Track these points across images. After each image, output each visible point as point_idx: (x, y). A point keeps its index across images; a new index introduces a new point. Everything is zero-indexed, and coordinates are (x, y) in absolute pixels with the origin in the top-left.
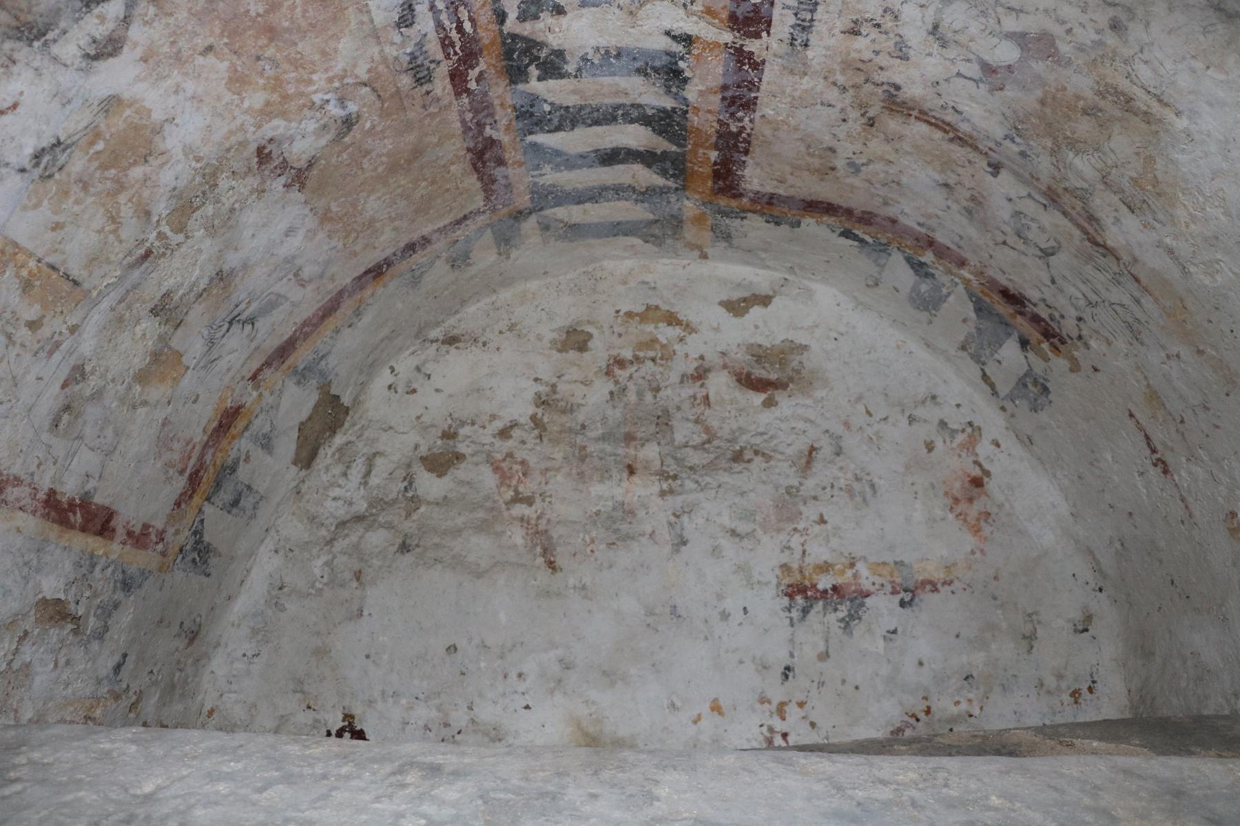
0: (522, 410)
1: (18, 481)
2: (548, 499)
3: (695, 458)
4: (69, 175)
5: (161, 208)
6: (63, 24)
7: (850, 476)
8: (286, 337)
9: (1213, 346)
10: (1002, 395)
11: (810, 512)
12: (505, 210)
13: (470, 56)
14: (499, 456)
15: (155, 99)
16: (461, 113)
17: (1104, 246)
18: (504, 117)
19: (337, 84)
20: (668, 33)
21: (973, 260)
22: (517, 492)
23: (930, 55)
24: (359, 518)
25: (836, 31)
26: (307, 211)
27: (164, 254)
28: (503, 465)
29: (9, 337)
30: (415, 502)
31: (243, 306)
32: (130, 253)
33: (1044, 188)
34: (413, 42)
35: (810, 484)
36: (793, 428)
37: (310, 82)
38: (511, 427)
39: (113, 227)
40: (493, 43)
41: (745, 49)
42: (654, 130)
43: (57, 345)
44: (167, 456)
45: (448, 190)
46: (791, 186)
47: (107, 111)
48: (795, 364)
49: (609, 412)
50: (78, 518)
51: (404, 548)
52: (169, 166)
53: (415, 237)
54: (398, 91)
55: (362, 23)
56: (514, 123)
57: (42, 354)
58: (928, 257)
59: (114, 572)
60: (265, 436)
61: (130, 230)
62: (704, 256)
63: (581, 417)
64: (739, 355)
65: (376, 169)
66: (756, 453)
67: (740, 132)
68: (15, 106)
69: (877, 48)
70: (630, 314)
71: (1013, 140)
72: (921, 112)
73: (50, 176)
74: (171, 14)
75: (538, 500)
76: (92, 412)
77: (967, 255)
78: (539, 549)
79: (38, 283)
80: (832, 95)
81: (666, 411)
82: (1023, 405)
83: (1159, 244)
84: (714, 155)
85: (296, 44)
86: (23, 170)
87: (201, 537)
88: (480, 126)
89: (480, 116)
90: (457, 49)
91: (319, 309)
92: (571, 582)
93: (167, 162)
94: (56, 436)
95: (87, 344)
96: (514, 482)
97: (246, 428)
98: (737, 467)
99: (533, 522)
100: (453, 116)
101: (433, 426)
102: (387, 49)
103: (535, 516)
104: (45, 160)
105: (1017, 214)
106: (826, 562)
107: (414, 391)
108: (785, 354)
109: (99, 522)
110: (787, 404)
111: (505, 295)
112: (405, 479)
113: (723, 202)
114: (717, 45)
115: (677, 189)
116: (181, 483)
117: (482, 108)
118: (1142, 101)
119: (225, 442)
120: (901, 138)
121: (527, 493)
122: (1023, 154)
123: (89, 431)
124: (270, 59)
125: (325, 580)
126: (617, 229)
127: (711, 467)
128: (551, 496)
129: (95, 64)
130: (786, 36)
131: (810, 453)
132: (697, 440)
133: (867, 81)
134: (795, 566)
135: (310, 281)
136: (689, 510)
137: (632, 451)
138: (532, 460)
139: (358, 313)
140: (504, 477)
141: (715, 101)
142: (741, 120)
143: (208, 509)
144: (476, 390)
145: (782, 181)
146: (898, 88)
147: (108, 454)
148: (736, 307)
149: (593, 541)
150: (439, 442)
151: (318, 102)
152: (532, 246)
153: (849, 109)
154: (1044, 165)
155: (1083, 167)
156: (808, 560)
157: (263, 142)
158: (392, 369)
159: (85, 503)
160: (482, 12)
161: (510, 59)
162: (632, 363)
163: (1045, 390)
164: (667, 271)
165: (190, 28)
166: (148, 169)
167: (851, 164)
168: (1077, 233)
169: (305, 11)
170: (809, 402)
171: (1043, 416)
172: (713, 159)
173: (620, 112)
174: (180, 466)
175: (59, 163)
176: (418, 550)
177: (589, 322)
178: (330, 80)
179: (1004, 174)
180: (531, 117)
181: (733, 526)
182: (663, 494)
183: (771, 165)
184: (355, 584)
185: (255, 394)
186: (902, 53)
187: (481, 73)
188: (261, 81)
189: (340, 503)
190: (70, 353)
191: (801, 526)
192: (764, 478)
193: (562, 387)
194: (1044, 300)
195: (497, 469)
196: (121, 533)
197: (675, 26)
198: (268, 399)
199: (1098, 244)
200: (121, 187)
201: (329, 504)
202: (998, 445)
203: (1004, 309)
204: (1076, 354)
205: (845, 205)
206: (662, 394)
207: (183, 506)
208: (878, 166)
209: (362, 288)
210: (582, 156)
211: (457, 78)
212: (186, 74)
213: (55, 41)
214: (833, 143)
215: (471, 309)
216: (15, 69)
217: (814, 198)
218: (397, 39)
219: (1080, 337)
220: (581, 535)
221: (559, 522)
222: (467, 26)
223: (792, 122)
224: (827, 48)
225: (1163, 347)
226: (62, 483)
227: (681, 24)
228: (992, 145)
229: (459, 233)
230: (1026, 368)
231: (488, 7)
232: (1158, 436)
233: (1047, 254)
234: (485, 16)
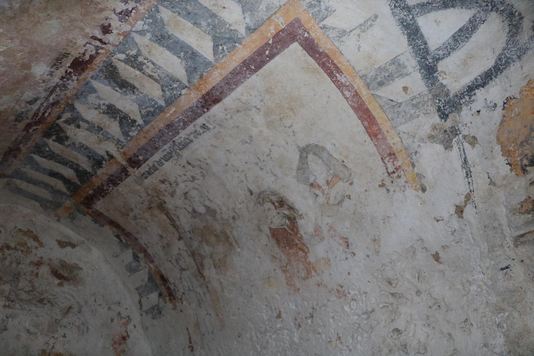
3: (24, 296)
7: (81, 322)
9: (222, 315)
10: (143, 310)
11: (61, 331)
17: (202, 274)
18: (30, 144)
21: (157, 262)
23: (180, 199)
25: (158, 179)
33: (192, 250)
35: (65, 320)
36: (66, 297)
58: (141, 255)
62: (58, 221)
66: (49, 302)
67: (106, 190)
69: (166, 189)
70: (20, 230)
71: (190, 233)
77: (155, 260)
80: (144, 195)
81: (19, 274)
82: (150, 315)
83: (218, 280)
84: (91, 192)
88: (21, 142)
90: (37, 119)
98: (39, 305)
105: (179, 254)
106: (60, 353)
110: (67, 288)
113: (82, 207)
114: (119, 163)
115: (68, 195)
117: (26, 138)
118: (231, 239)
122: (191, 238)
126: (35, 198)
127: (29, 302)
130: (142, 172)
131: (69, 309)
132: (27, 289)
133: (157, 196)
134: (48, 351)
136: (13, 316)
141: (105, 178)
142: (109, 187)
145: (108, 211)
146: (165, 203)
148: (62, 244)
154: (195, 244)
155: (207, 249)
156: (53, 350)
163: (160, 312)
164: (42, 220)
168: (196, 267)
170: (75, 289)
171: (155, 322)
172: (90, 193)
179: (182, 242)
182: (5, 306)
186: (172, 195)
187: (37, 129)
191: (56, 336)
192: (48, 313)
194: (174, 284)
199: (200, 273)
202: (135, 327)
203: (158, 281)
204: (177, 304)
205: (124, 227)
206: (20, 266)
208: (143, 221)
210: (44, 169)
218: (23, 105)
219: (181, 299)
222: (46, 114)
224: (152, 182)
225: (207, 310)
227: (113, 152)
228: (183, 232)
230: (157, 303)
232: (194, 338)
233: (182, 270)
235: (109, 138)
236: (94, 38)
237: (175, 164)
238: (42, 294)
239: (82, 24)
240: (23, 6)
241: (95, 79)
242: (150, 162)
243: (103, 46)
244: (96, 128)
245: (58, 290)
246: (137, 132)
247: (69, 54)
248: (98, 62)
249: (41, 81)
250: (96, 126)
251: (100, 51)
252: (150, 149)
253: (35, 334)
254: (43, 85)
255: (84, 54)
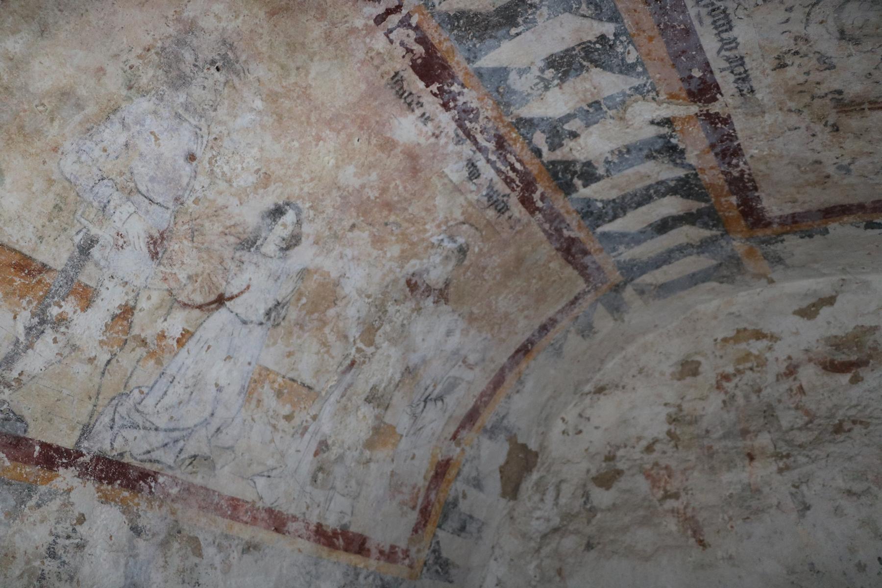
0: (660, 429)
1: (295, 518)
2: (690, 492)
3: (802, 437)
4: (290, 321)
5: (354, 332)
6: (263, 235)
8: (470, 407)
12: (605, 287)
13: (528, 185)
14: (648, 467)
15: (330, 265)
16: (540, 225)
18: (573, 220)
19: (444, 228)
20: (652, 123)
22: (666, 491)
23: (849, 56)
24: (555, 530)
25: (768, 71)
26: (456, 317)
27: (364, 362)
28: (652, 472)
29: (274, 426)
30: (592, 511)
31: (431, 389)
32: (341, 364)
34: (485, 187)
37: (425, 231)
38: (654, 443)
39: (325, 349)
40: (540, 172)
41: (711, 112)
42: (682, 196)
43: (306, 429)
44: (399, 497)
45: (554, 281)
46: (804, 203)
47: (302, 279)
48: (870, 343)
49: (726, 416)
50: (341, 542)
51: (589, 546)
52: (350, 305)
53: (544, 319)
54: (488, 221)
55: (445, 184)
56: (582, 222)
57: (297, 436)
59: (374, 580)
60: (475, 479)
61: (338, 350)
62: (771, 281)
63: (704, 424)
64: (820, 349)
65: (494, 278)
68: (248, 287)
69: (806, 69)
70: (725, 340)
72: (870, 103)
73: (278, 325)
74: (323, 212)
75: (683, 494)
76: (338, 471)
78: (690, 532)
79: (286, 391)
80: (793, 120)
81: (770, 406)
85: (406, 209)
86: (261, 324)
87: (440, 554)
88: (559, 231)
89: (555, 224)
90: (517, 182)
91: (490, 383)
92: (720, 554)
93: (349, 302)
94: (317, 488)
95: (326, 426)
96: (662, 484)
97: (458, 474)
98: (840, 437)
99: (682, 511)
100: (535, 228)
101: (597, 454)
102: (469, 196)
103: (682, 507)
104: (273, 314)
107: (580, 432)
108: (858, 338)
109: (357, 545)
111: (631, 349)
112: (583, 496)
113: (760, 233)
115: (722, 235)
116: (414, 516)
117: (554, 218)
119: (443, 486)
120: (867, 130)
121: (674, 490)
123: (339, 484)
124: (394, 223)
125: (537, 579)
126: (694, 280)
127: (817, 442)
128: (691, 489)
129: (287, 252)
132: (800, 422)
133: (813, 98)
135: (476, 364)
136: (806, 480)
137: (748, 443)
138: (673, 464)
139: (521, 382)
140: (654, 482)
141: (711, 159)
142: (737, 166)
143: (441, 534)
144: (624, 422)
146: (840, 92)
147: (356, 498)
148: (808, 312)
149: (731, 519)
150: (604, 465)
151: (436, 243)
152: (638, 312)
153: (812, 125)
157: (409, 277)
158: (563, 420)
159: (344, 532)
160: (524, 153)
161: (557, 178)
162: (735, 375)
164: (745, 300)
165: (336, 217)
166: (337, 309)
167: (840, 168)
169: (405, 187)
172: (735, 203)
173: (652, 191)
174: (411, 504)
175: (282, 315)
176: (600, 546)
177: (696, 353)
178: (439, 226)
180: (592, 215)
181: (848, 487)
182: (780, 471)
183: (779, 192)
184: (558, 579)
185: (458, 450)
187: (542, 195)
188: (393, 238)
189: (542, 521)
190: (316, 433)
192: (867, 442)
193: (685, 406)
195: (648, 476)
196: (374, 552)
197: (654, 116)
198: (469, 452)
200: (324, 323)
201: (534, 523)
206: (764, 393)
207: (420, 532)
208: (863, 161)
209: (517, 363)
210: (642, 232)
211: (526, 202)
212: (344, 245)
213: (262, 245)
214: (816, 156)
215: (610, 365)
216: (244, 266)
217: (827, 205)
218: (473, 188)
220: (721, 515)
221: (701, 508)
222: (518, 166)
223: (776, 152)
224: (769, 86)
226: (326, 519)
227: (658, 113)
229: (576, 311)
231: (526, 150)
234: (527, 156)
235: (623, 102)
236: (380, 19)
237: (748, 16)
238: (831, 416)
239: (344, 28)
240: (264, 96)
241: (475, 57)
242: (717, 64)
243: (404, 12)
244: (591, 110)
245: (856, 392)
246: (631, 47)
247: (397, 74)
248: (436, 35)
249: (433, 140)
250: (586, 108)
251: (414, 21)
252: (682, 45)
253: (867, 491)
254: (443, 140)
255: (409, 51)
